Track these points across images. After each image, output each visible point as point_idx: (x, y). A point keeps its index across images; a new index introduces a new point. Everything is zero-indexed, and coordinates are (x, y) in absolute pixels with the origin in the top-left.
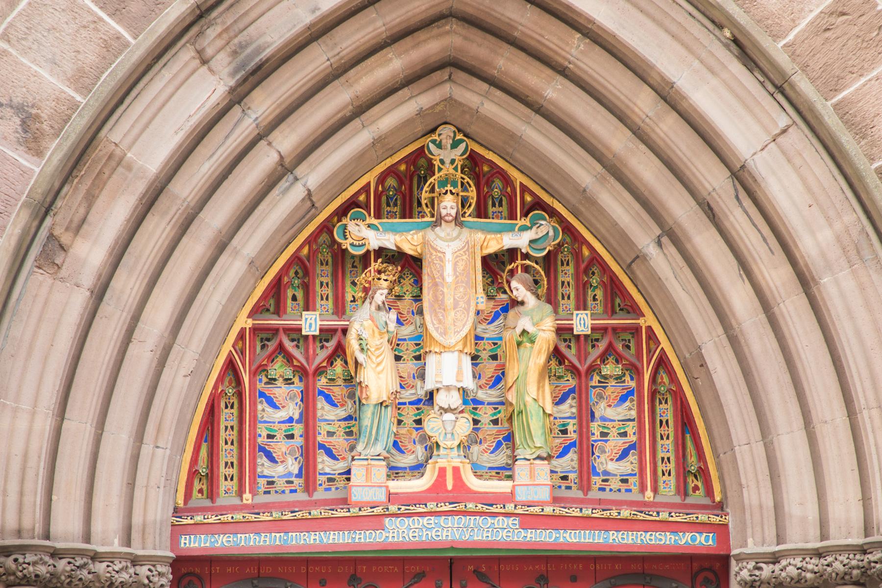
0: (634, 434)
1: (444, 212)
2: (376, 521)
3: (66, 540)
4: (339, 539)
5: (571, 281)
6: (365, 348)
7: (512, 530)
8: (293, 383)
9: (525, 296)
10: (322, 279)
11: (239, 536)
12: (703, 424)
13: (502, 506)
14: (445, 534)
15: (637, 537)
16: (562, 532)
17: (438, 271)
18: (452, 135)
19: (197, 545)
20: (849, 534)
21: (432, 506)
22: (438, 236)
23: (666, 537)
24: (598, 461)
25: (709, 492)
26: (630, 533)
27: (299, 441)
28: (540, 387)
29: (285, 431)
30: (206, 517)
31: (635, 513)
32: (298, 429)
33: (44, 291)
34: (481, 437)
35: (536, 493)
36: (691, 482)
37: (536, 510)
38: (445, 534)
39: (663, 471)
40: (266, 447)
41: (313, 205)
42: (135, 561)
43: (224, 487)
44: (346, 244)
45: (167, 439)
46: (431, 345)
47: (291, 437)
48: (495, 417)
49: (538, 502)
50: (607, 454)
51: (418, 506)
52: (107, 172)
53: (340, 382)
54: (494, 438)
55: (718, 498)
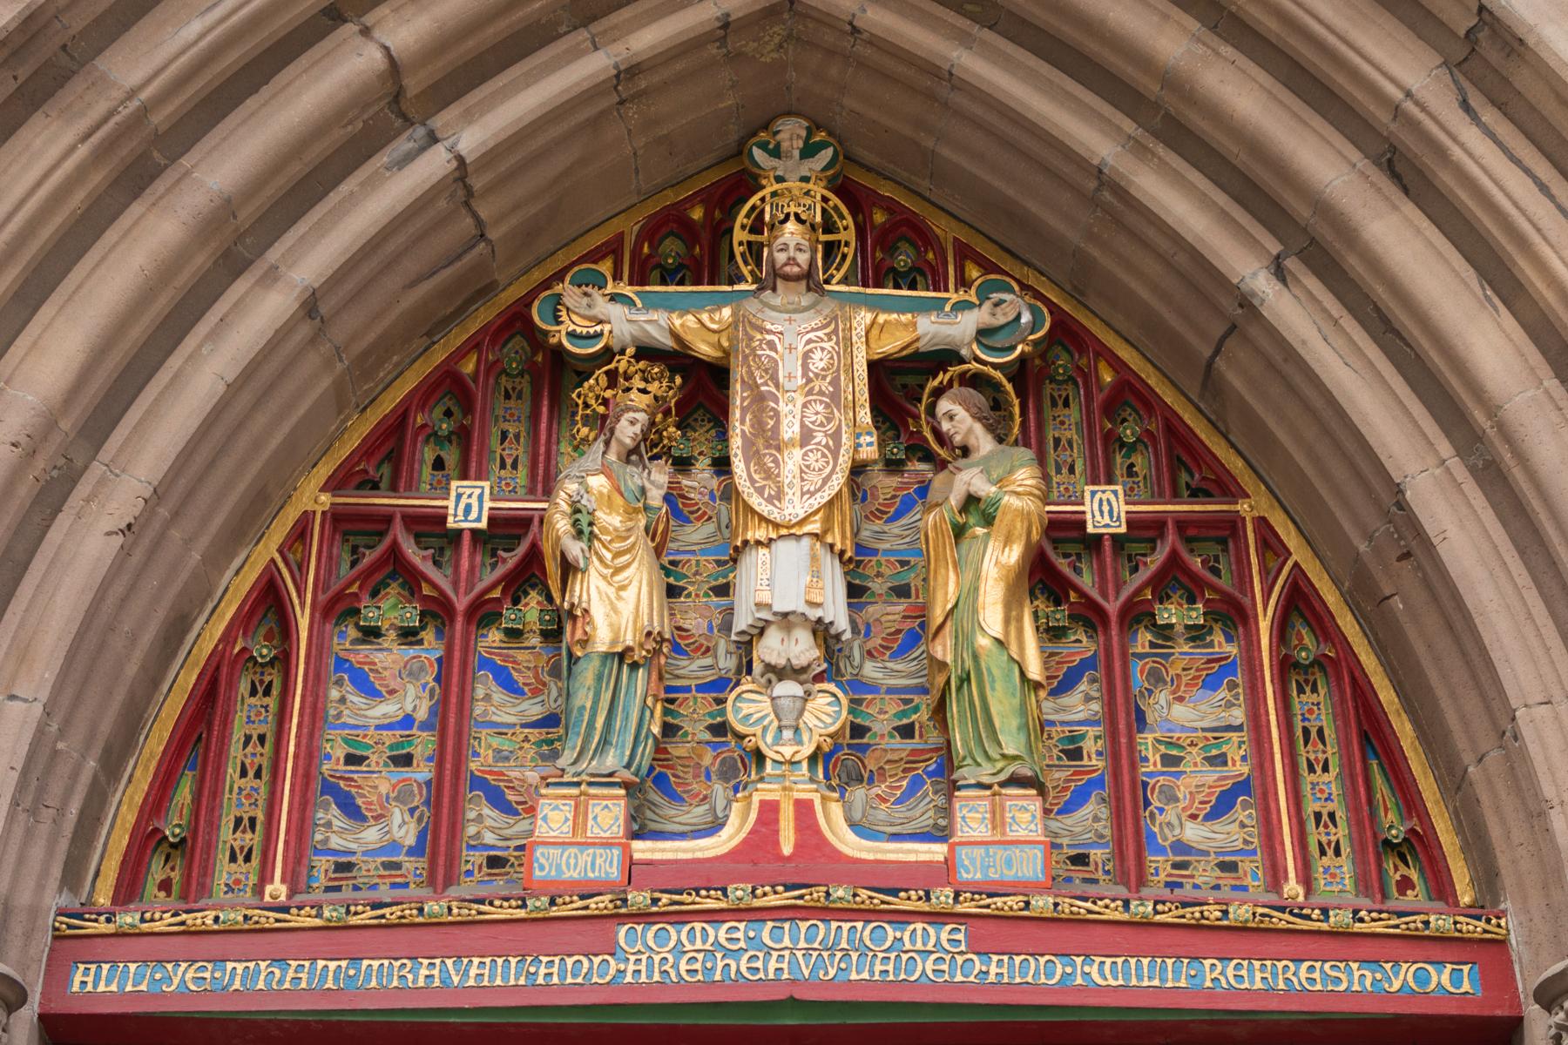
0: (1244, 758)
1: (781, 258)
4: (492, 977)
5: (1075, 437)
6: (586, 530)
7: (948, 958)
8: (421, 642)
9: (970, 431)
10: (506, 426)
11: (230, 965)
12: (1408, 726)
13: (921, 893)
14: (773, 965)
15: (1275, 975)
16: (1079, 960)
17: (766, 371)
18: (804, 133)
19: (114, 988)
21: (740, 893)
22: (766, 305)
23: (1351, 973)
24: (1159, 818)
25: (1441, 889)
26: (1257, 964)
27: (422, 772)
28: (1011, 616)
29: (392, 747)
30: (148, 916)
31: (1266, 911)
32: (423, 744)
34: (872, 766)
35: (1009, 863)
37: (1013, 902)
38: (773, 965)
39: (1320, 844)
40: (342, 783)
41: (482, 236)
43: (225, 875)
44: (560, 335)
46: (746, 529)
47: (406, 760)
48: (905, 721)
49: (1014, 884)
50: (1181, 805)
51: (703, 893)
54: (905, 771)
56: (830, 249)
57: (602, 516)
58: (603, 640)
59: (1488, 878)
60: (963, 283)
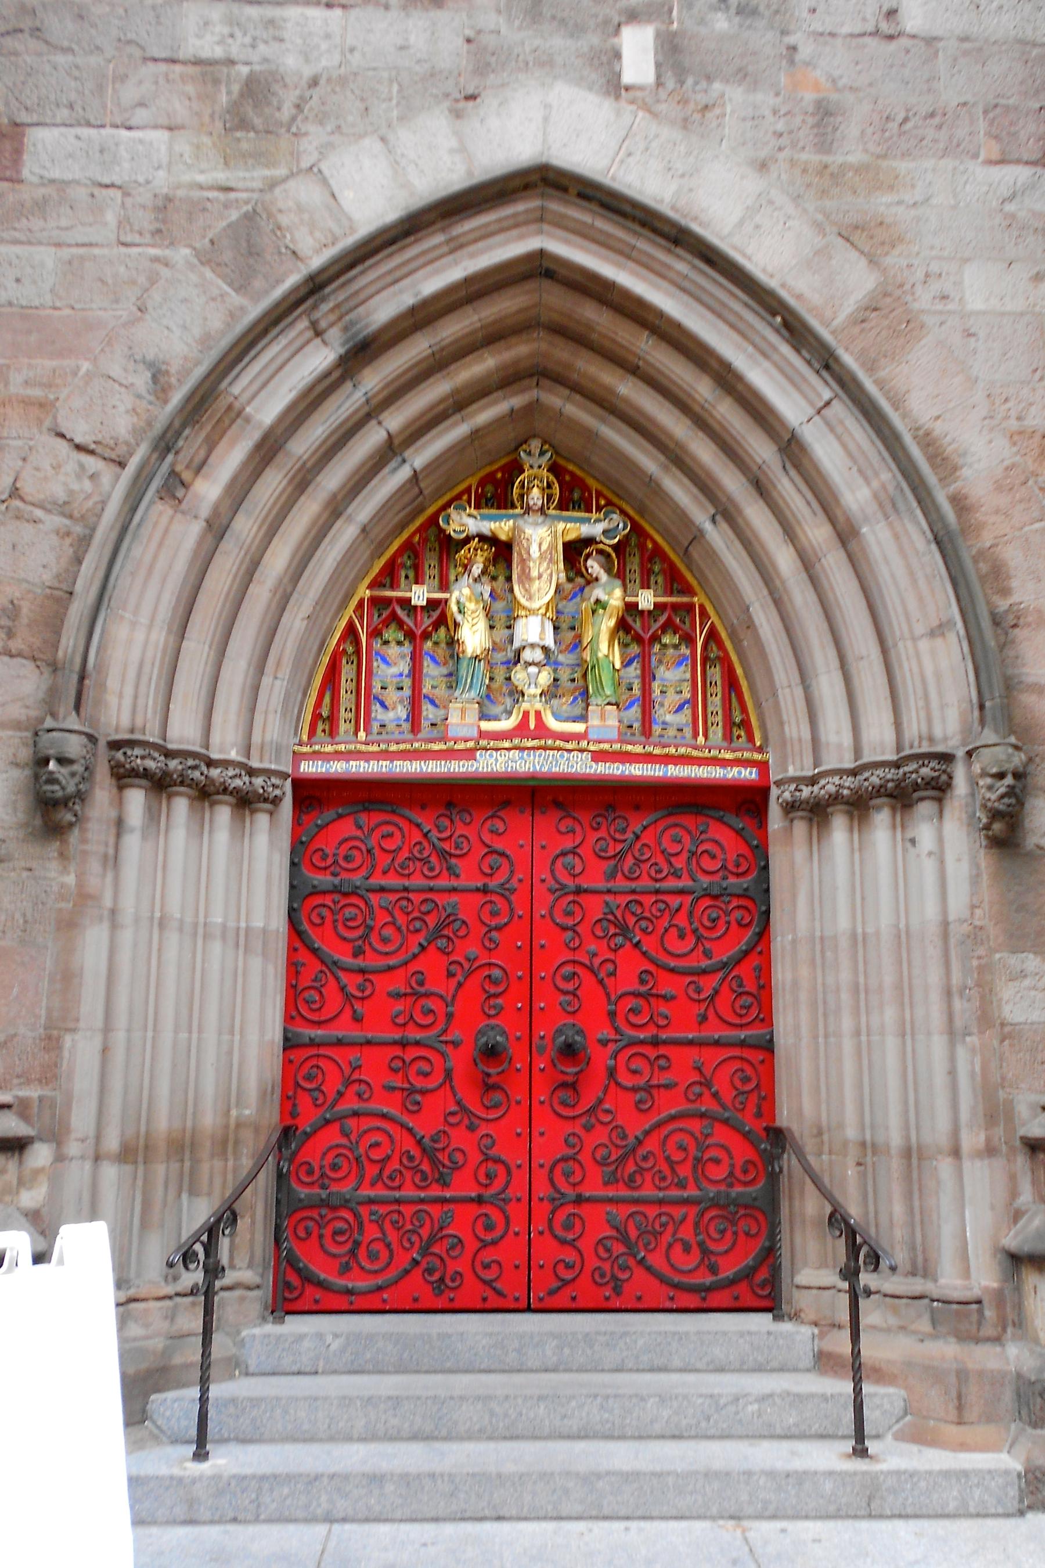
1: (531, 503)
2: (469, 754)
3: (181, 743)
20: (883, 753)
25: (751, 738)
27: (407, 692)
32: (407, 683)
33: (164, 520)
36: (736, 732)
37: (606, 746)
42: (252, 772)
45: (285, 671)
52: (227, 422)
53: (443, 645)
55: (758, 744)
56: (550, 498)
57: (468, 604)
58: (469, 652)
59: (765, 738)
60: (599, 509)
